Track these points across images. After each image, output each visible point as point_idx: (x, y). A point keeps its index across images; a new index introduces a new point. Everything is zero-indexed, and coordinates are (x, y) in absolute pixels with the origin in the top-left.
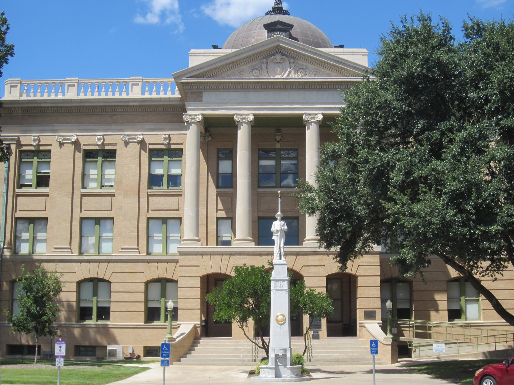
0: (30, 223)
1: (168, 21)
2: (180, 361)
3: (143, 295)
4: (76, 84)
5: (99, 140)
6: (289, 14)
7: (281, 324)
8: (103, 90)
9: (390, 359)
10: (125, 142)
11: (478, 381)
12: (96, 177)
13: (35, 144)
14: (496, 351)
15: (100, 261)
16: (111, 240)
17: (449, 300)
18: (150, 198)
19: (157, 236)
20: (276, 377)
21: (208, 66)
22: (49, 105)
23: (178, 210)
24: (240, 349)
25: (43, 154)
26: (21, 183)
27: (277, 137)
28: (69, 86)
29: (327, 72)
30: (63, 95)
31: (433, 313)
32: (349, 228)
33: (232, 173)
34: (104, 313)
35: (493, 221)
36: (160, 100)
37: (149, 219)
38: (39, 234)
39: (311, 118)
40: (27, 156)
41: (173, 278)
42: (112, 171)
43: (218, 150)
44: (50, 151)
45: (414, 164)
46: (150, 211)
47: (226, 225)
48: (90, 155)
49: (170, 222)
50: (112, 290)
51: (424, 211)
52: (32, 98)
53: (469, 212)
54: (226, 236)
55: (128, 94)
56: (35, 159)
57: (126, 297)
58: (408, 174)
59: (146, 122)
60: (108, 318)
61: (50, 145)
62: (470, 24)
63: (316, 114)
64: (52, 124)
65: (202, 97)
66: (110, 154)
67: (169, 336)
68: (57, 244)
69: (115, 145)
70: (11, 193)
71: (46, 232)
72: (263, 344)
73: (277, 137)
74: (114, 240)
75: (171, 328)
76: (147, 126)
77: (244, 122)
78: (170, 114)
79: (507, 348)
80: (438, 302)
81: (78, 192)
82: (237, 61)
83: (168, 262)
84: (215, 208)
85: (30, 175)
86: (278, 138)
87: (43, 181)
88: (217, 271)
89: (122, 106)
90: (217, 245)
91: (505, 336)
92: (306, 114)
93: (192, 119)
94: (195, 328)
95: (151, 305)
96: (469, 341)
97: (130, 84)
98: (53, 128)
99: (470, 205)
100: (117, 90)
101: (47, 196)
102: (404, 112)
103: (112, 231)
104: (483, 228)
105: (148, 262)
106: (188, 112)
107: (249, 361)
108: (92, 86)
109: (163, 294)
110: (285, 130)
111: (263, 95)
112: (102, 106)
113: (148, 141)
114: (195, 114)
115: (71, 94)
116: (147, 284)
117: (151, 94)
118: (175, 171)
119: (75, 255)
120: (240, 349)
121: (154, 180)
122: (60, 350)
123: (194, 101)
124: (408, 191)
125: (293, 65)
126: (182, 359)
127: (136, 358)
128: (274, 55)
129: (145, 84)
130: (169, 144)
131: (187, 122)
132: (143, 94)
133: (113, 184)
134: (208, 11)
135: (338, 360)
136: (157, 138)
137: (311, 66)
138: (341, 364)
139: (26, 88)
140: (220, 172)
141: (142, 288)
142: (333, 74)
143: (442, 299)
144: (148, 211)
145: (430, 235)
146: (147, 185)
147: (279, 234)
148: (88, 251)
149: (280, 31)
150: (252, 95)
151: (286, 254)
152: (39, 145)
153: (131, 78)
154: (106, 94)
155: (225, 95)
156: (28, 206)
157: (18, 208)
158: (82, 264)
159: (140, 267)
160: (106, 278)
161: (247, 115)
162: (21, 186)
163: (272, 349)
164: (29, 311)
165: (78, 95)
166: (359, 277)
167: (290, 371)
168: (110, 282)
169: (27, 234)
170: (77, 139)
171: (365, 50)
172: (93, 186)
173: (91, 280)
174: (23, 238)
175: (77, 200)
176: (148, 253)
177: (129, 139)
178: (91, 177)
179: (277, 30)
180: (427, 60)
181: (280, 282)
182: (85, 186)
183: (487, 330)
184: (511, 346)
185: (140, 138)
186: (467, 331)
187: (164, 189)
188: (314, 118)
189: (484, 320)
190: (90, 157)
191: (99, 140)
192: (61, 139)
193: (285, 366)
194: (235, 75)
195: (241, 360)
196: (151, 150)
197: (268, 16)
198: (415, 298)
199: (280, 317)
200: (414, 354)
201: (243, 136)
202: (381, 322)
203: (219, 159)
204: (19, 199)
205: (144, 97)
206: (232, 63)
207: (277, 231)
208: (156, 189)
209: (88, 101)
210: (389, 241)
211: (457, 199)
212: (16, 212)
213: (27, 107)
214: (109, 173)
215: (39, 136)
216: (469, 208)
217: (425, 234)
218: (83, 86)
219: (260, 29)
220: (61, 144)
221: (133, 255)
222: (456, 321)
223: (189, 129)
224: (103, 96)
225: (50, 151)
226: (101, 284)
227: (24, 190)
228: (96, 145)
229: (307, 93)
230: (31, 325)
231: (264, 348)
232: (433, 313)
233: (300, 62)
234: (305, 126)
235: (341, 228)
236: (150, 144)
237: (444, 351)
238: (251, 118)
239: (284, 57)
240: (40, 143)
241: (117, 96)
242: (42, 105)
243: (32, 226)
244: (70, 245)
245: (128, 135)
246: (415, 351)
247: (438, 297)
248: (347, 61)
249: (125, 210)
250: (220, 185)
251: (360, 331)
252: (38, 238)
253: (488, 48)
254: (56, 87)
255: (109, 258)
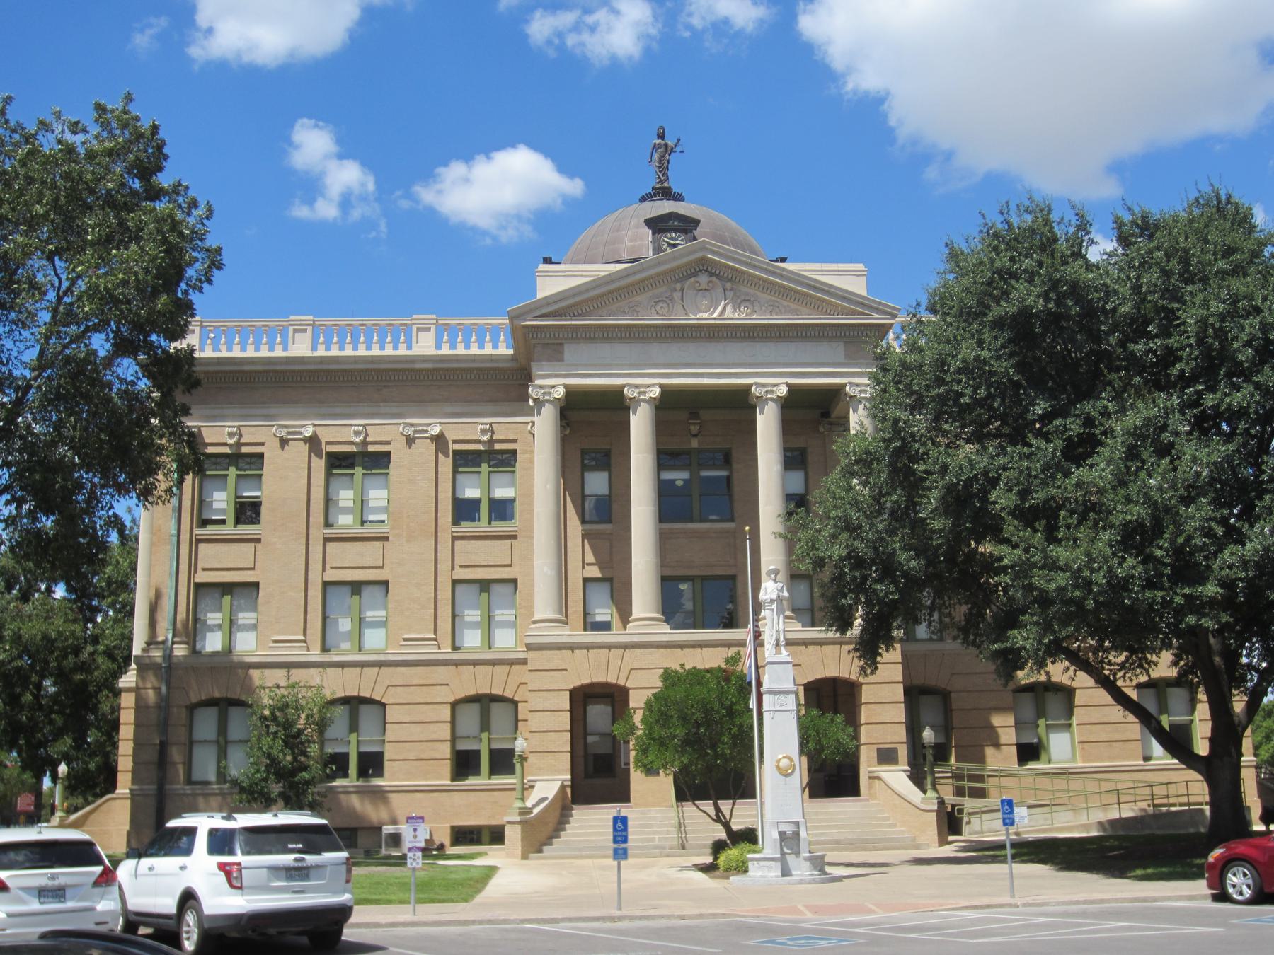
0: (223, 594)
1: (356, 214)
2: (540, 851)
3: (448, 726)
4: (310, 329)
5: (357, 433)
6: (683, 200)
7: (786, 775)
8: (335, 339)
9: (936, 837)
10: (407, 438)
11: (1217, 872)
12: (351, 504)
13: (231, 442)
14: (1121, 819)
15: (362, 665)
16: (383, 624)
17: (1018, 725)
18: (457, 543)
19: (472, 615)
20: (783, 875)
21: (574, 296)
22: (259, 368)
23: (510, 566)
24: (650, 826)
25: (248, 462)
26: (205, 517)
27: (692, 428)
28: (296, 331)
29: (793, 306)
30: (285, 349)
31: (989, 752)
32: (892, 593)
33: (610, 496)
34: (372, 764)
35: (1202, 580)
36: (474, 358)
37: (455, 582)
38: (241, 615)
39: (767, 392)
40: (216, 465)
41: (506, 694)
42: (383, 493)
43: (584, 453)
44: (261, 456)
45: (1034, 473)
46: (456, 567)
47: (600, 595)
48: (339, 462)
49: (496, 588)
50: (388, 719)
51: (1075, 560)
52: (224, 354)
53: (1158, 561)
54: (603, 613)
55: (409, 348)
56: (232, 472)
57: (416, 732)
58: (1024, 494)
59: (447, 400)
60: (379, 772)
61: (262, 444)
62: (1127, 218)
63: (775, 385)
64: (264, 403)
65: (562, 353)
66: (376, 461)
67: (519, 804)
68: (278, 633)
69: (388, 443)
70: (185, 536)
71: (255, 609)
72: (717, 815)
73: (692, 428)
74: (389, 623)
75: (524, 789)
76: (449, 409)
77: (644, 400)
78: (505, 385)
79: (1139, 814)
80: (999, 730)
81: (317, 533)
82: (627, 287)
83: (493, 663)
84: (583, 562)
85: (221, 501)
86: (694, 429)
87: (248, 511)
88: (602, 679)
89: (400, 370)
90: (585, 630)
91: (1132, 791)
92: (758, 385)
93: (544, 394)
94: (563, 787)
95: (463, 746)
96: (1065, 801)
97: (414, 328)
98: (265, 412)
99: (1161, 548)
100: (389, 339)
101: (258, 541)
102: (1010, 380)
103: (513, 605)
104: (1187, 591)
105: (457, 664)
106: (538, 382)
107: (671, 849)
108: (467, 331)
109: (485, 725)
110: (705, 415)
111: (675, 350)
112: (362, 370)
113: (450, 437)
114: (551, 385)
115: (301, 348)
116: (454, 705)
117: (453, 347)
118: (501, 493)
119: (315, 655)
120: (650, 826)
121: (464, 510)
122: (415, 837)
123: (549, 360)
124: (1040, 525)
125: (730, 294)
126: (545, 848)
127: (437, 849)
128: (695, 275)
129: (442, 329)
130: (491, 441)
131: (535, 400)
132: (439, 347)
133: (383, 517)
134: (427, 195)
135: (838, 842)
136: (469, 430)
137: (764, 297)
138: (846, 850)
139: (212, 335)
140: (587, 492)
141: (446, 713)
142: (804, 310)
143: (1004, 724)
144: (453, 568)
145: (1090, 604)
146: (450, 520)
147: (774, 606)
148: (338, 646)
149: (676, 231)
150: (655, 350)
151: (789, 643)
152: (239, 444)
153: (415, 317)
154: (369, 348)
155: (605, 350)
156: (219, 562)
157: (200, 566)
158: (346, 670)
159: (441, 673)
160: (508, 694)
161: (649, 386)
162: (204, 523)
163: (773, 823)
164: (274, 761)
165: (314, 348)
166: (864, 687)
167: (808, 863)
168: (384, 705)
169: (219, 615)
170: (315, 433)
171: (860, 266)
172: (345, 521)
173: (346, 701)
174: (209, 622)
175: (316, 549)
176: (455, 648)
177: (415, 432)
178: (342, 504)
179: (670, 230)
180: (1055, 285)
181: (782, 697)
182: (331, 520)
183: (1099, 780)
184: (1144, 810)
185: (435, 431)
186: (1060, 783)
187: (482, 526)
188: (772, 392)
189: (1084, 761)
190: (339, 467)
191: (357, 433)
192: (283, 433)
193: (797, 853)
194: (624, 313)
195: (656, 847)
196: (456, 453)
197: (648, 204)
198: (956, 722)
199: (784, 763)
200: (966, 829)
201: (640, 426)
202: (908, 768)
203: (585, 468)
204: (202, 547)
205: (440, 353)
206: (618, 289)
207: (772, 601)
208: (466, 527)
209: (457, 359)
210: (936, 616)
211: (1135, 538)
212: (196, 571)
213: (217, 372)
214: (377, 496)
215: (239, 427)
216: (1159, 553)
217: (1080, 604)
218: (324, 332)
219: (637, 227)
220: (283, 442)
221: (428, 651)
222: (1031, 765)
223: (539, 413)
224: (362, 351)
225: (261, 456)
226: (496, 708)
227: (210, 531)
228: (351, 443)
229: (758, 346)
230: (276, 788)
231: (718, 820)
232: (989, 752)
233: (743, 289)
234: (755, 408)
235: (877, 595)
236: (454, 442)
237: (1026, 821)
238: (656, 392)
239: (714, 279)
240: (368, 439)
241: (389, 351)
242: (246, 368)
243: (227, 599)
244: (305, 634)
245: (412, 425)
246: (969, 823)
247: (997, 720)
248: (831, 286)
249: (410, 565)
250: (587, 518)
251: (870, 787)
252: (240, 622)
253: (1168, 261)
254: (396, 331)
255: (382, 658)
